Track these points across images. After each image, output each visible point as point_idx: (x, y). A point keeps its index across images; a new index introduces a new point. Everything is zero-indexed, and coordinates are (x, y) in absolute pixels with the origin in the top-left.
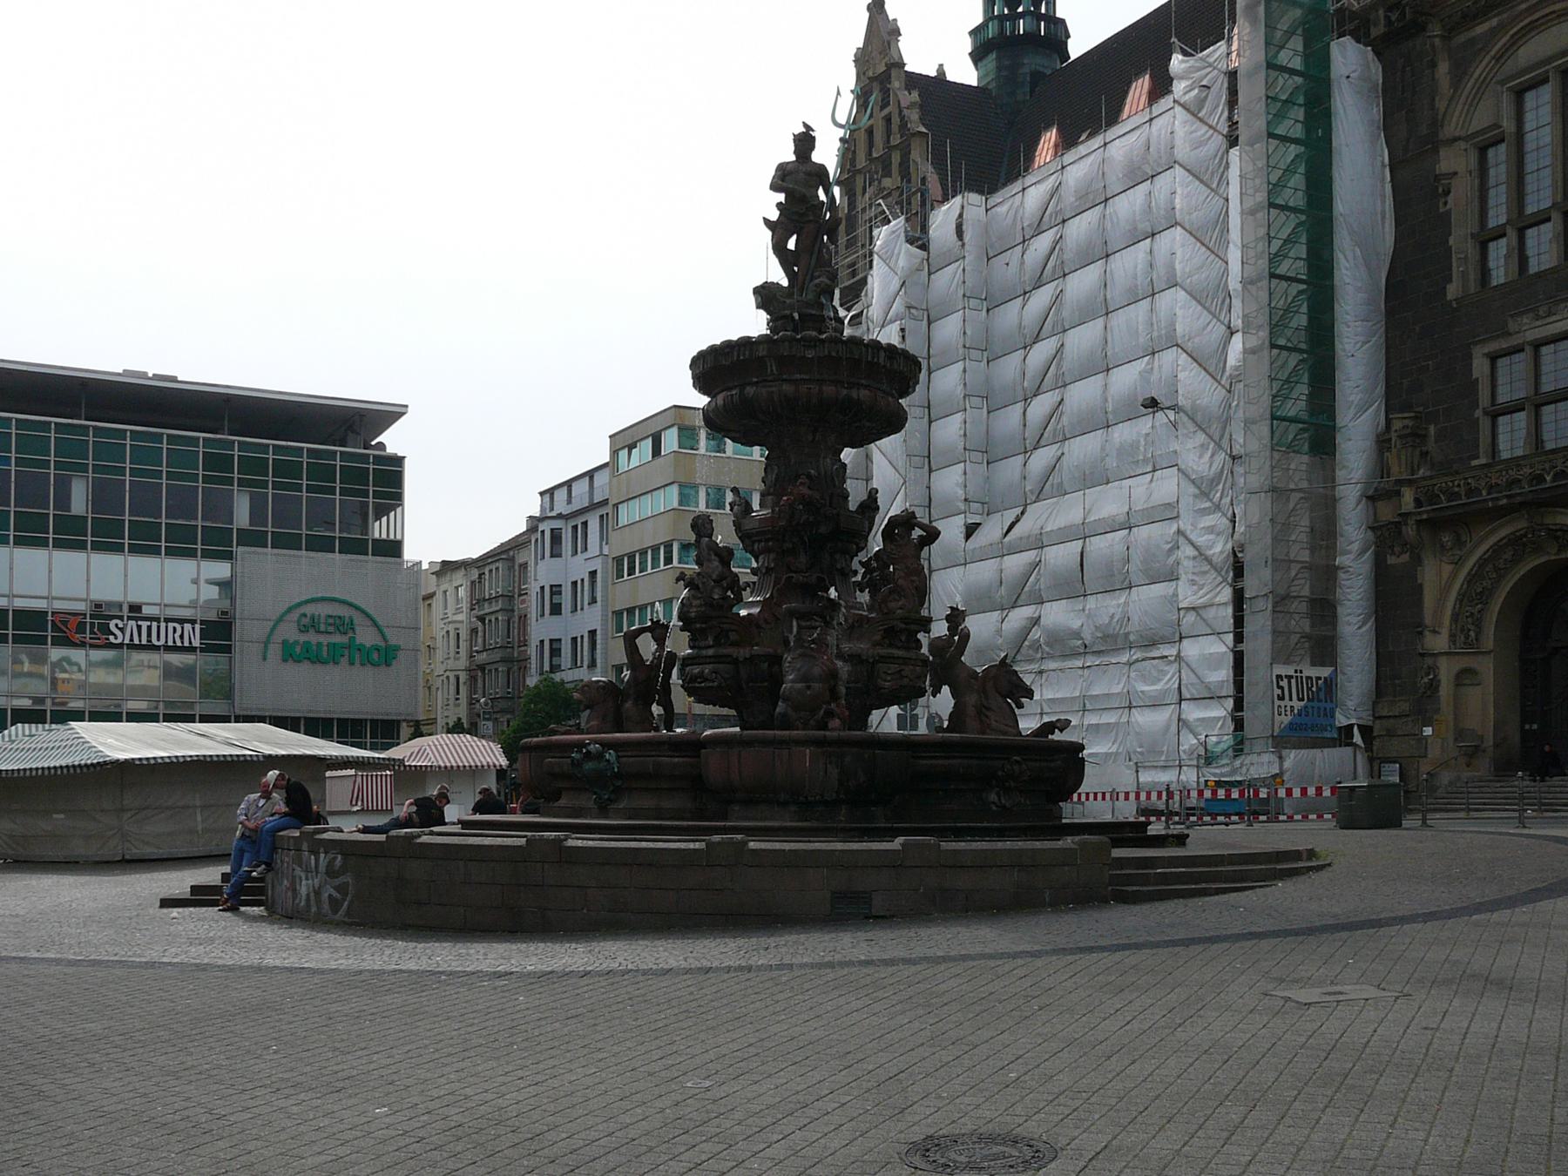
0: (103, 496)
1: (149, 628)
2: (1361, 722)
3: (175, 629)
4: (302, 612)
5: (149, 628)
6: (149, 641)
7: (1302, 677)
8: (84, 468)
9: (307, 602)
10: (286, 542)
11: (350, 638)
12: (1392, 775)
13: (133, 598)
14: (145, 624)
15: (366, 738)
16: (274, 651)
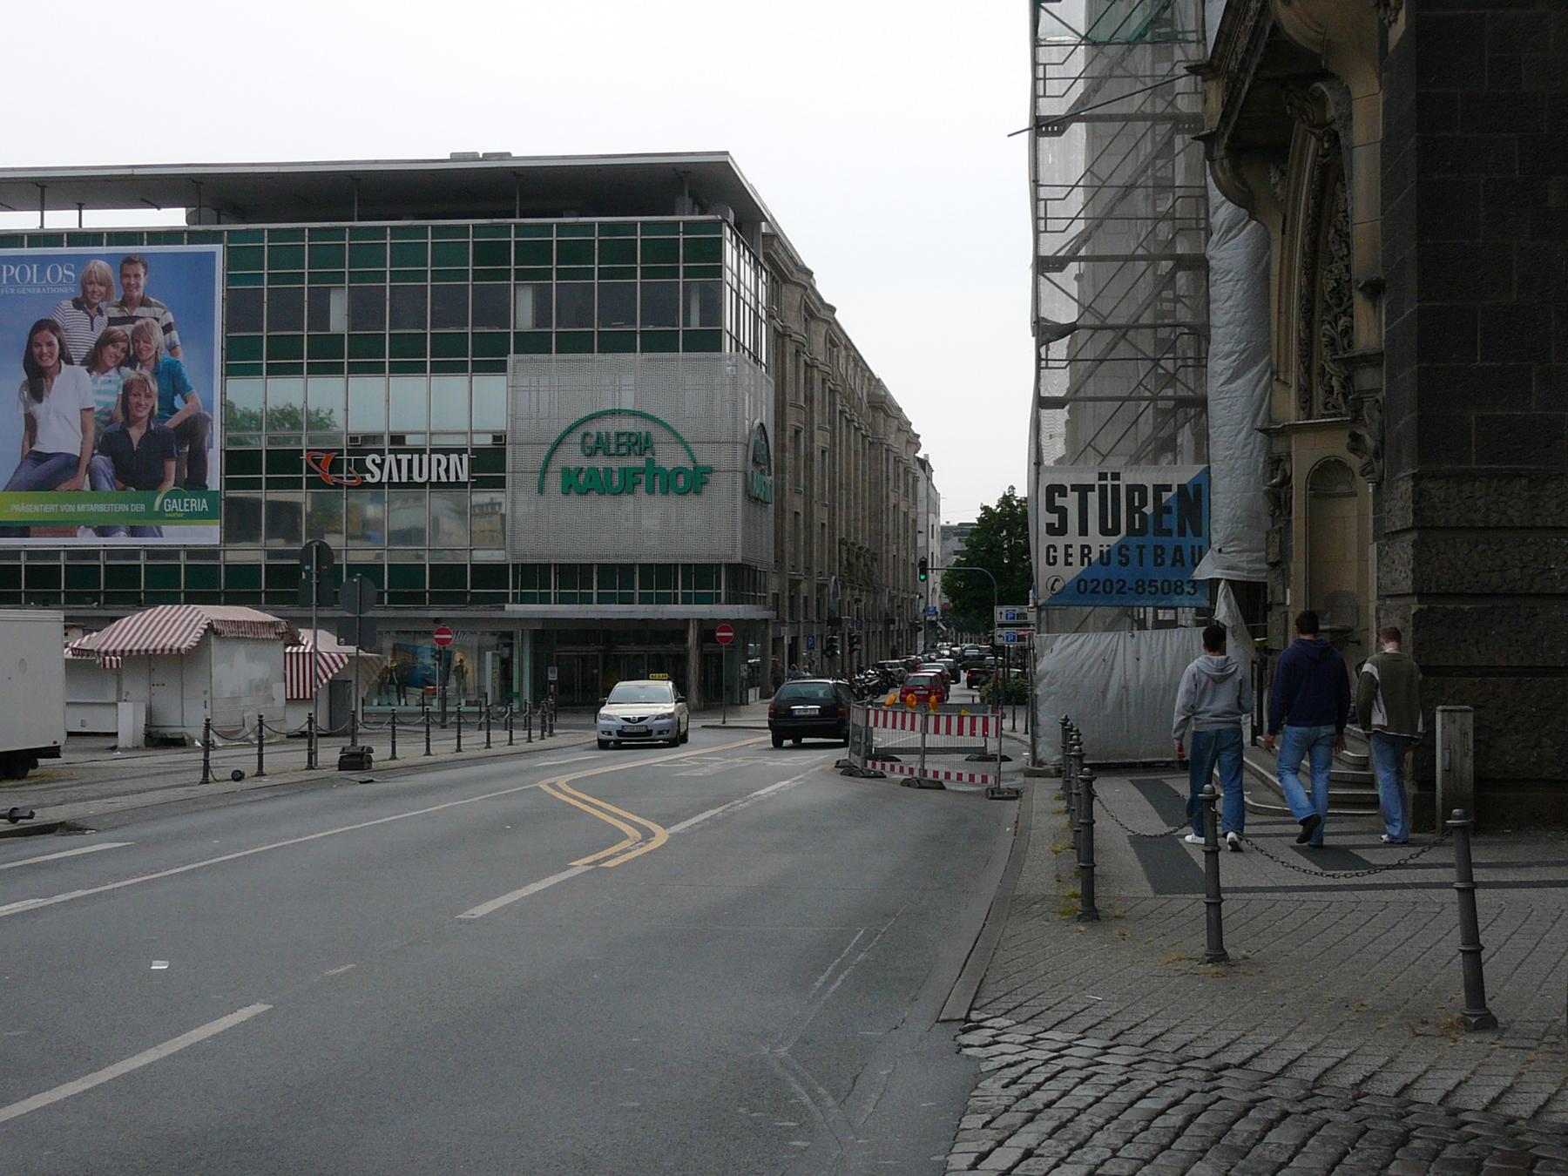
0: (363, 309)
1: (410, 462)
2: (1235, 575)
3: (439, 461)
4: (584, 430)
5: (410, 462)
6: (410, 477)
7: (1116, 489)
8: (339, 277)
9: (592, 418)
10: (574, 344)
13: (396, 428)
14: (404, 458)
15: (719, 587)
16: (554, 481)
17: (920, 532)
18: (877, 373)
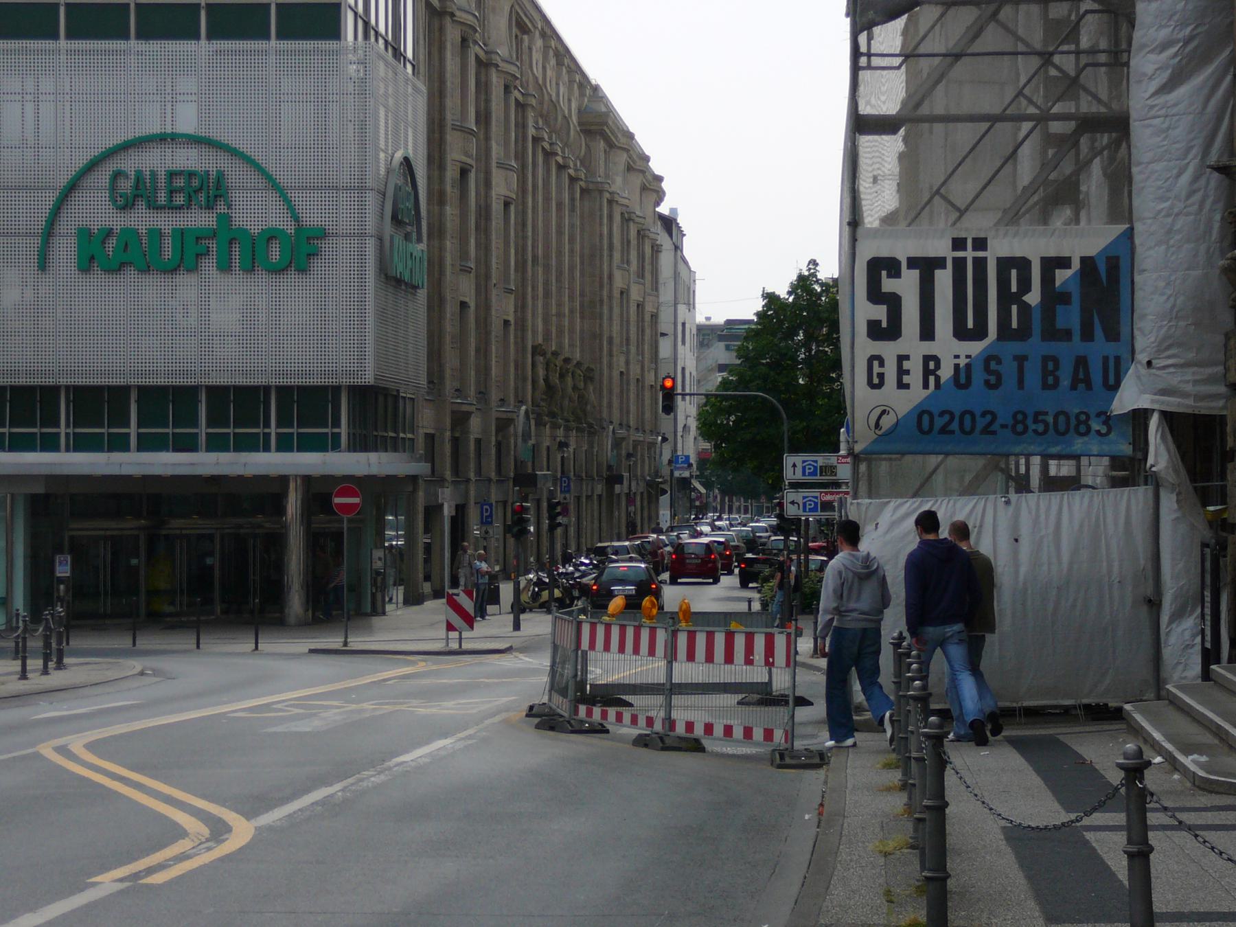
2: (1174, 404)
7: (980, 264)
9: (126, 147)
11: (219, 216)
12: (576, 593)
15: (267, 425)
16: (65, 250)
17: (663, 335)
18: (594, 71)
